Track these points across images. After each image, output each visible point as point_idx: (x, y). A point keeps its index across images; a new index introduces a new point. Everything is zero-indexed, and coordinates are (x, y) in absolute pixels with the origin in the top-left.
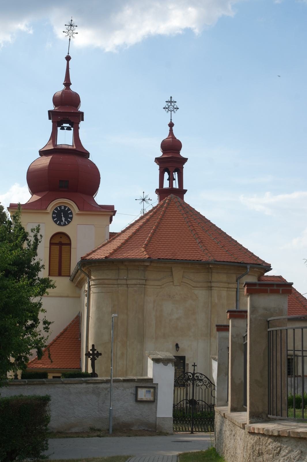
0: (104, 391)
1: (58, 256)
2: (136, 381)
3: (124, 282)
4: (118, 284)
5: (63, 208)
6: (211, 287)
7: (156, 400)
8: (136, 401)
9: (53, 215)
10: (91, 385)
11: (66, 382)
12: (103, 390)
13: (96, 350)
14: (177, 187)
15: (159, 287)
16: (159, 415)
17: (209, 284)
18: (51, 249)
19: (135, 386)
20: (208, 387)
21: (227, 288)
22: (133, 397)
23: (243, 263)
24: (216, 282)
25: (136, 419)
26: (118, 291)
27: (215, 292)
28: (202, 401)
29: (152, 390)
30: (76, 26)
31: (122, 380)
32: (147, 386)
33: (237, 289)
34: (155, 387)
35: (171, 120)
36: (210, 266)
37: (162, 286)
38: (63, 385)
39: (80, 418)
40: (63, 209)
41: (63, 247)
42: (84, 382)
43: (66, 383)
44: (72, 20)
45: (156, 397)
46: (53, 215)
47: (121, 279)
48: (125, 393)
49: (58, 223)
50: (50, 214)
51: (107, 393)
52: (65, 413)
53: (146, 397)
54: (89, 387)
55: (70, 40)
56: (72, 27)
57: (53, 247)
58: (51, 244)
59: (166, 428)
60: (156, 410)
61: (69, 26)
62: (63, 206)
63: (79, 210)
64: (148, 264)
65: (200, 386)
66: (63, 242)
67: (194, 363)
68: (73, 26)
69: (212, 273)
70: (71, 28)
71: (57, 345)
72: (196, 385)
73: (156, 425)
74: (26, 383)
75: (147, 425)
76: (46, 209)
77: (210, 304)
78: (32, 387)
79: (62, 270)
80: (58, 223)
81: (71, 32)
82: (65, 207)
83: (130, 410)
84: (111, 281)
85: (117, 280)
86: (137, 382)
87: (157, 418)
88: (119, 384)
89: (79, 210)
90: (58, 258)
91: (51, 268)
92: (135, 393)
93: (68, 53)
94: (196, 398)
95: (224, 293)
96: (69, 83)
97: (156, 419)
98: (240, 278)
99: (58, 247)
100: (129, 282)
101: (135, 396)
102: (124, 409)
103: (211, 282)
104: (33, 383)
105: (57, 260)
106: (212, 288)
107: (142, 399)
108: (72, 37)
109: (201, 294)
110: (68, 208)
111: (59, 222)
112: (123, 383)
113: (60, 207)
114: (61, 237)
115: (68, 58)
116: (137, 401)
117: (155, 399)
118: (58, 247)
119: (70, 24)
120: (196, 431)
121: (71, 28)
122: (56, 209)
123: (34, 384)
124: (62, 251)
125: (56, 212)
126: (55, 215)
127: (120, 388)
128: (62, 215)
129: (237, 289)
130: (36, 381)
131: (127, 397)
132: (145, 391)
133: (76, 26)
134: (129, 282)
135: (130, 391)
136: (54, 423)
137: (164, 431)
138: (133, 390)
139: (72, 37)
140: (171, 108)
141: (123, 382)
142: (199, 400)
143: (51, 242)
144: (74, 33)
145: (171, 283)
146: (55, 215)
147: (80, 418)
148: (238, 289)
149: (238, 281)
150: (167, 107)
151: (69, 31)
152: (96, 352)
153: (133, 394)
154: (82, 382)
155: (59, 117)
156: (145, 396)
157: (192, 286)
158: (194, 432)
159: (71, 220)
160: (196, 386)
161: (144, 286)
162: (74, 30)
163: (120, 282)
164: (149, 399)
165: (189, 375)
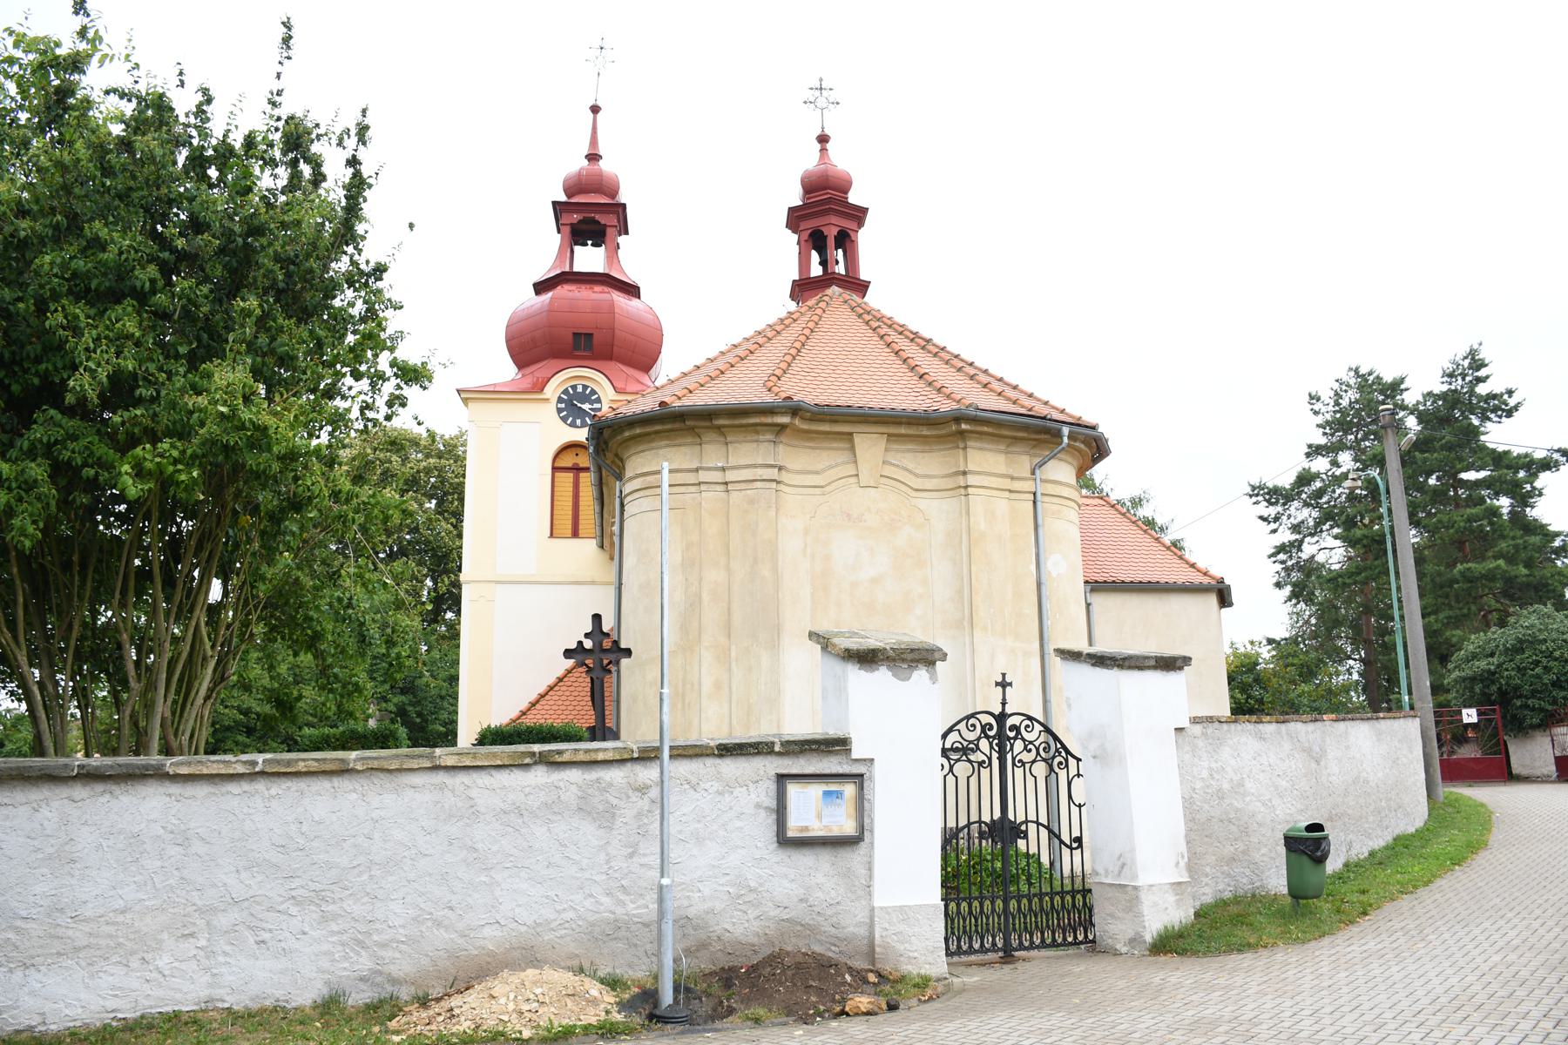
0: (634, 799)
2: (777, 748)
3: (716, 476)
4: (699, 484)
5: (580, 389)
6: (966, 487)
7: (866, 834)
8: (778, 842)
9: (559, 406)
10: (574, 774)
11: (449, 763)
12: (629, 797)
13: (580, 643)
14: (843, 272)
15: (817, 491)
16: (882, 898)
17: (961, 481)
19: (772, 773)
20: (1057, 769)
21: (1010, 491)
22: (768, 823)
23: (1050, 420)
24: (979, 473)
25: (783, 920)
27: (978, 500)
28: (1038, 824)
29: (849, 789)
31: (712, 748)
32: (827, 771)
33: (1035, 494)
34: (862, 775)
35: (823, 128)
36: (964, 426)
37: (828, 489)
38: (441, 777)
39: (523, 929)
41: (582, 475)
42: (535, 763)
43: (454, 768)
45: (867, 821)
46: (559, 406)
47: (709, 469)
48: (731, 808)
51: (646, 808)
52: (451, 909)
53: (825, 821)
54: (561, 784)
58: (555, 469)
59: (916, 954)
60: (871, 877)
64: (785, 420)
65: (1028, 766)
66: (581, 465)
67: (1004, 675)
69: (965, 448)
71: (564, 688)
72: (1014, 759)
73: (872, 945)
74: (257, 769)
75: (835, 945)
77: (965, 537)
78: (289, 788)
79: (581, 527)
82: (585, 387)
83: (753, 884)
84: (679, 475)
85: (697, 470)
86: (779, 754)
87: (877, 913)
88: (702, 766)
92: (774, 804)
93: (593, 157)
94: (1017, 814)
95: (1002, 504)
97: (872, 918)
98: (1041, 465)
100: (731, 476)
101: (774, 816)
102: (728, 878)
103: (964, 473)
104: (289, 770)
106: (970, 490)
107: (806, 829)
109: (938, 510)
112: (718, 761)
113: (575, 387)
116: (785, 841)
117: (861, 828)
120: (1021, 947)
122: (566, 392)
123: (298, 774)
126: (563, 406)
127: (707, 786)
129: (1035, 494)
130: (304, 760)
131: (739, 824)
132: (821, 793)
134: (731, 476)
135: (753, 796)
136: (397, 955)
137: (910, 968)
138: (765, 793)
140: (821, 102)
141: (720, 756)
142: (1026, 822)
143: (556, 465)
145: (853, 480)
146: (563, 406)
147: (523, 929)
148: (1039, 495)
149: (1038, 472)
150: (812, 100)
152: (588, 644)
153: (767, 808)
154: (527, 761)
156: (819, 817)
157: (911, 488)
158: (1017, 954)
160: (1014, 764)
161: (774, 485)
163: (703, 476)
164: (836, 832)
165: (986, 724)
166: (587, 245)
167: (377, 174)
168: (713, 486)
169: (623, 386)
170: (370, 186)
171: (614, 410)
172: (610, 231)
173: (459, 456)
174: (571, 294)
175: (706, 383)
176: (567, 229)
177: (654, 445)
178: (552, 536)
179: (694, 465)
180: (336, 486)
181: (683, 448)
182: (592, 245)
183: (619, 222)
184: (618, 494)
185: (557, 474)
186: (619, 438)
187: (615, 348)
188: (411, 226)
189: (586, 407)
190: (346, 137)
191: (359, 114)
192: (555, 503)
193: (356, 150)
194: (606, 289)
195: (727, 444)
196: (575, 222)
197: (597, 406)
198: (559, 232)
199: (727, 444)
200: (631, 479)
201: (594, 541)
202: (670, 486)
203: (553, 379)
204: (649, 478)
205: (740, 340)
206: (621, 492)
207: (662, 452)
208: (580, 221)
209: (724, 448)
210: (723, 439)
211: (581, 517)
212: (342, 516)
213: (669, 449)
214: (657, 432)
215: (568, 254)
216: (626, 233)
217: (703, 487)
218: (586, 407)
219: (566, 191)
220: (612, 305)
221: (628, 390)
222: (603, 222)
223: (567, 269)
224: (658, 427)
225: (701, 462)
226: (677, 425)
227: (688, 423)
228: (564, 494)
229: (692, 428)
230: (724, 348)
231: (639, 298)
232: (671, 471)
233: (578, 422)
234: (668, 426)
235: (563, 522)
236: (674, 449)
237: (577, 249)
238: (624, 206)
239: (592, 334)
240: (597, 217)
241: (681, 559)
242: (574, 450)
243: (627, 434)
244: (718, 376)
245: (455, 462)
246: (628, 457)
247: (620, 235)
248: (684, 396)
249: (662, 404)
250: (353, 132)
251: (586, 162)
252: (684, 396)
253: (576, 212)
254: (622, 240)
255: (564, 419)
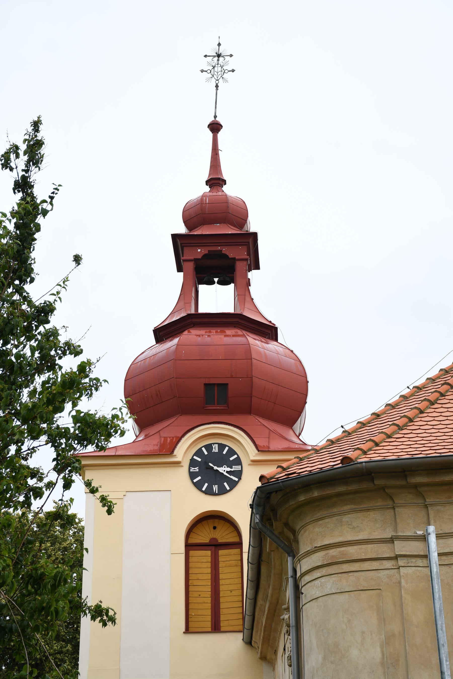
1: (210, 577)
4: (396, 558)
5: (215, 449)
9: (192, 469)
18: (190, 560)
26: (400, 583)
30: (231, 56)
40: (217, 451)
41: (221, 552)
44: (219, 45)
46: (192, 469)
49: (204, 489)
50: (182, 466)
55: (217, 86)
56: (221, 59)
57: (195, 554)
58: (189, 547)
61: (214, 56)
62: (217, 445)
63: (259, 451)
68: (223, 57)
70: (218, 60)
76: (173, 452)
79: (222, 618)
80: (204, 489)
81: (220, 69)
82: (222, 447)
84: (370, 546)
85: (391, 540)
89: (257, 452)
90: (210, 584)
91: (191, 613)
93: (215, 117)
96: (219, 179)
99: (209, 553)
105: (207, 589)
108: (221, 80)
110: (230, 449)
111: (206, 485)
113: (209, 447)
114: (215, 528)
115: (73, 270)
118: (209, 553)
119: (216, 53)
121: (218, 60)
122: (199, 453)
124: (220, 565)
125: (200, 460)
126: (197, 469)
128: (215, 468)
133: (231, 56)
139: (221, 80)
143: (191, 541)
144: (226, 71)
146: (197, 469)
151: (214, 67)
155: (199, 250)
159: (240, 479)
162: (227, 64)
166: (213, 283)
167: (52, 198)
168: (414, 560)
169: (266, 444)
170: (45, 213)
171: (284, 469)
172: (240, 266)
173: (56, 537)
174: (199, 339)
175: (394, 433)
176: (190, 266)
177: (335, 510)
178: (187, 631)
179: (388, 534)
180: (36, 569)
181: (372, 514)
182: (219, 283)
183: (249, 254)
184: (290, 573)
185: (192, 553)
186: (292, 503)
187: (254, 399)
188: (77, 259)
189: (223, 470)
190: (12, 156)
191: (30, 129)
192: (191, 588)
193: (27, 171)
194: (240, 332)
195: (426, 507)
196: (200, 257)
197: (236, 468)
198: (180, 269)
199: (426, 507)
200: (308, 553)
201: (240, 636)
202: (439, 555)
203: (183, 439)
204: (333, 552)
205: (423, 380)
206: (295, 571)
207: (346, 518)
208: (205, 256)
209: (423, 513)
210: (420, 501)
211: (222, 606)
212: (43, 608)
213: (354, 515)
214: (339, 495)
215: (193, 295)
216: (257, 267)
217: (401, 562)
218: (223, 470)
219: (187, 222)
220: (248, 348)
221: (272, 448)
222: (231, 256)
223: (193, 311)
224: (341, 489)
225: (396, 530)
226: (364, 485)
227: (377, 482)
228: (200, 576)
229: (383, 489)
230: (406, 392)
231: (276, 340)
232: (438, 536)
233: (215, 488)
234: (353, 487)
235: (200, 612)
236: (360, 515)
237: (202, 288)
238: (255, 235)
239: (227, 384)
240: (225, 250)
241: (380, 655)
242: (211, 523)
243: (302, 498)
244: (406, 425)
245: (53, 544)
246: (303, 527)
247: (250, 270)
248: (370, 449)
249: (346, 460)
250: (23, 147)
251: (207, 189)
252: (370, 449)
253: (199, 247)
254: (253, 275)
255: (198, 486)
